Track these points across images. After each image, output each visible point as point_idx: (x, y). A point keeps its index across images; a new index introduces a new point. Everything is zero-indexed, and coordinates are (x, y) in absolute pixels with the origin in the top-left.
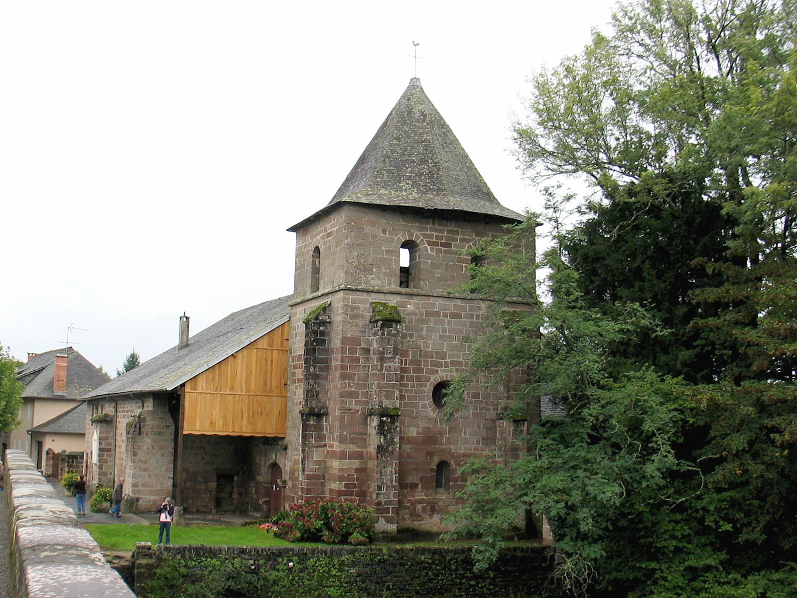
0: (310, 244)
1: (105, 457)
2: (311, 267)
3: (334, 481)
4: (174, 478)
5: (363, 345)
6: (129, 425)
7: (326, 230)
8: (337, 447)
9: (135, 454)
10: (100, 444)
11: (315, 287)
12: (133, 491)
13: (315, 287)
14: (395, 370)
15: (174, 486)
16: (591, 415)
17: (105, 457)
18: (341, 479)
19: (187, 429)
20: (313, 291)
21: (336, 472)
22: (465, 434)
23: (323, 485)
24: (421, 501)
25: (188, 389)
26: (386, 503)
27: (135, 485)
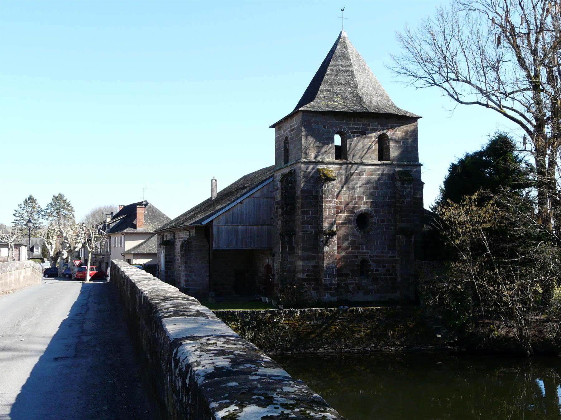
0: (283, 135)
1: (169, 266)
2: (284, 149)
3: (300, 273)
4: (209, 276)
5: (314, 194)
6: (182, 246)
7: (291, 127)
8: (300, 253)
9: (186, 263)
10: (166, 258)
11: (286, 161)
12: (186, 285)
13: (286, 161)
14: (333, 208)
15: (209, 281)
16: (364, 204)
17: (169, 266)
18: (304, 272)
19: (215, 247)
20: (285, 164)
21: (301, 268)
22: (377, 244)
23: (294, 276)
24: (352, 284)
25: (214, 223)
26: (330, 285)
27: (186, 281)
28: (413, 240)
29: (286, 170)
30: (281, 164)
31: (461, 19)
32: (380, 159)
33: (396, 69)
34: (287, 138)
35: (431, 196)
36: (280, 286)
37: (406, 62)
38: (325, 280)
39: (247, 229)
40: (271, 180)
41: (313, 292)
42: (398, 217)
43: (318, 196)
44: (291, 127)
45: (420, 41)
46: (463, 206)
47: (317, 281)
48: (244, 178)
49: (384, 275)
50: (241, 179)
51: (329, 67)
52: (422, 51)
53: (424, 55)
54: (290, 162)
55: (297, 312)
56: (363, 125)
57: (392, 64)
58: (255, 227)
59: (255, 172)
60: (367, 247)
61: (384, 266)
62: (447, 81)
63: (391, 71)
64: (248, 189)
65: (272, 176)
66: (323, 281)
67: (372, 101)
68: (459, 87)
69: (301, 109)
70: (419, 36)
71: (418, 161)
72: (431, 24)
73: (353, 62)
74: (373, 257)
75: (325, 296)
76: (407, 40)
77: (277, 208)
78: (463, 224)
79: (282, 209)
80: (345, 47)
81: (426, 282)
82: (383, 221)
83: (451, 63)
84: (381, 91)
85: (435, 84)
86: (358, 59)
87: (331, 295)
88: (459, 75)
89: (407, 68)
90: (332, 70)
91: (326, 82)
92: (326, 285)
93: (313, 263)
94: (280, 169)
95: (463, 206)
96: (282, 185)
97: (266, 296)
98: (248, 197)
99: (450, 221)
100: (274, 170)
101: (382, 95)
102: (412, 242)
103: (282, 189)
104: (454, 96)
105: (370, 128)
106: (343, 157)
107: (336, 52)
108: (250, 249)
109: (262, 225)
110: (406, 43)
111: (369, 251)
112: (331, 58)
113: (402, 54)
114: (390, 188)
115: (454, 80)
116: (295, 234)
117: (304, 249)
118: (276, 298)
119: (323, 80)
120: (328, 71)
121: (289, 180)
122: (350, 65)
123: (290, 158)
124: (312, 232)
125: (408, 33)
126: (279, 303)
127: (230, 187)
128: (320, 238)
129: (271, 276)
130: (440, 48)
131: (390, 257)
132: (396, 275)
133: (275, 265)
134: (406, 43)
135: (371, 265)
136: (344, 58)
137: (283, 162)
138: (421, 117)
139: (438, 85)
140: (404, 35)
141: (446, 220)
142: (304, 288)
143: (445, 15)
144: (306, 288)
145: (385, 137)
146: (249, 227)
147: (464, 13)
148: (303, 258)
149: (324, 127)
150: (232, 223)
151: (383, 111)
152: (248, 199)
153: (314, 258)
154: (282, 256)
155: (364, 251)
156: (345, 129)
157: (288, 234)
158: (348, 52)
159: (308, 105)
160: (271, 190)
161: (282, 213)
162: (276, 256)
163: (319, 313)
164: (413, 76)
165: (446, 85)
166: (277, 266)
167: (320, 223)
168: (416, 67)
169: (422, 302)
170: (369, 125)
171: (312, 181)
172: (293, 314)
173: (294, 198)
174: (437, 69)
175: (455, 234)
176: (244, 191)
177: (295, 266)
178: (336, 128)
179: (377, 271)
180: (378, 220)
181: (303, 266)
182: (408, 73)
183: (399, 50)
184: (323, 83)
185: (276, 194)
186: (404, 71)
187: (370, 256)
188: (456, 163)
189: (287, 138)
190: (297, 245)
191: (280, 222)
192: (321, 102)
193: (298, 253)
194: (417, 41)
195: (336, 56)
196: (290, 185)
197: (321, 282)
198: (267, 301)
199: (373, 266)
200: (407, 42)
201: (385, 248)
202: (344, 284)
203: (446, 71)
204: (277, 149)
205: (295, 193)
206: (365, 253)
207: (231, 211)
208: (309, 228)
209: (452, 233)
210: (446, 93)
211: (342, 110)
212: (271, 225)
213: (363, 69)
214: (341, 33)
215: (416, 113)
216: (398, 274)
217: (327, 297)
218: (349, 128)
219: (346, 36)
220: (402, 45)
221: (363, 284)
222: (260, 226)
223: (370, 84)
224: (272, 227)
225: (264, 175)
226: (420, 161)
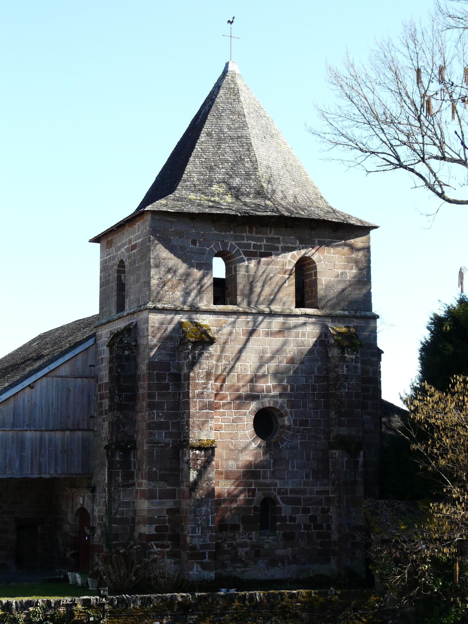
0: (114, 258)
2: (118, 284)
3: (144, 524)
5: (173, 370)
7: (130, 241)
8: (144, 484)
11: (121, 307)
13: (121, 307)
18: (151, 521)
20: (117, 313)
21: (145, 514)
22: (293, 467)
24: (244, 545)
26: (202, 547)
28: (361, 459)
29: (121, 325)
30: (110, 313)
31: (448, 44)
32: (299, 304)
33: (328, 136)
34: (122, 262)
35: (399, 377)
36: (105, 550)
37: (347, 123)
38: (194, 537)
39: (41, 439)
40: (91, 342)
41: (168, 561)
42: (333, 414)
43: (179, 375)
44: (130, 241)
45: (374, 84)
46: (453, 394)
47: (177, 539)
48: (41, 337)
49: (307, 527)
50: (34, 340)
51: (204, 130)
52: (377, 102)
53: (380, 111)
54: (128, 309)
55: (134, 602)
56: (268, 240)
57: (321, 126)
58: (58, 435)
59: (62, 328)
60: (273, 473)
61: (305, 511)
62: (423, 160)
63: (318, 139)
64: (46, 359)
65: (94, 335)
66: (188, 540)
67: (288, 195)
68: (445, 171)
69: (148, 208)
70: (373, 75)
71: (369, 307)
72: (393, 53)
73: (250, 120)
74: (286, 492)
75: (192, 569)
76: (348, 81)
77: (102, 397)
78: (451, 429)
79: (111, 399)
80: (235, 93)
81: (384, 542)
82: (304, 423)
83: (430, 127)
84: (301, 176)
85: (401, 165)
86: (260, 114)
87: (205, 567)
88: (447, 149)
89: (350, 135)
90: (209, 134)
91: (198, 157)
92: (193, 548)
93: (169, 504)
94: (109, 322)
95: (453, 394)
96: (111, 353)
97: (76, 571)
98: (46, 375)
99: (429, 425)
100: (97, 323)
101: (303, 184)
102: (360, 463)
103: (111, 361)
104: (437, 189)
105: (281, 245)
106: (228, 299)
107: (217, 100)
108: (47, 476)
109: (71, 430)
110: (345, 87)
111: (278, 481)
112: (207, 113)
113: (339, 107)
114: (317, 360)
115: (437, 158)
116: (134, 448)
117: (151, 477)
118: (96, 575)
119: (193, 154)
120: (203, 137)
121: (126, 342)
122: (244, 125)
123: (127, 300)
124: (167, 445)
125: (351, 69)
126: (101, 584)
127: (12, 355)
128: (184, 454)
129: (88, 532)
130: (409, 97)
131: (318, 492)
132: (329, 527)
133: (96, 509)
134: (345, 87)
135: (280, 509)
136: (233, 113)
137: (114, 309)
138: (376, 227)
139: (406, 167)
140: (344, 72)
141: (419, 422)
142: (151, 553)
143: (419, 37)
144: (155, 553)
145: (309, 264)
146: (47, 435)
147: (455, 33)
148: (150, 495)
149: (194, 243)
150: (14, 425)
151: (304, 214)
152: (44, 379)
153: (171, 495)
154: (109, 491)
155: (268, 481)
156: (233, 247)
157: (122, 447)
158: (239, 101)
159: (163, 201)
160: (91, 362)
161: (110, 406)
162: (98, 489)
163: (179, 603)
164: (361, 150)
165: (421, 168)
166: (100, 511)
167: (183, 425)
168: (365, 134)
169: (377, 580)
170: (278, 241)
171: (169, 345)
172: (127, 605)
173: (134, 378)
174: (404, 139)
175: (438, 449)
176: (38, 364)
177: (135, 511)
178: (216, 246)
179: (292, 519)
180: (295, 421)
181: (149, 511)
182: (350, 143)
183: (334, 101)
184: (191, 159)
185: (100, 369)
186: (343, 139)
187: (280, 489)
188: (441, 313)
189: (122, 262)
190: (139, 470)
191: (106, 424)
192: (187, 197)
193: (140, 485)
194: (369, 84)
195: (217, 109)
196: (127, 353)
197: (185, 540)
198: (79, 581)
199: (286, 510)
200: (350, 86)
201: (307, 476)
202: (230, 545)
203: (420, 140)
204: (103, 284)
205: (136, 367)
206: (270, 485)
207: (11, 403)
208: (162, 437)
209: (433, 445)
210: (422, 183)
211: (227, 212)
212: (89, 430)
213: (269, 134)
214: (227, 64)
215: (367, 218)
216: (333, 527)
217: (195, 571)
218: (240, 245)
219: (237, 72)
220: (338, 91)
221: (266, 546)
222: (68, 433)
223: (281, 164)
224: (91, 434)
225: (79, 334)
226: (375, 310)
